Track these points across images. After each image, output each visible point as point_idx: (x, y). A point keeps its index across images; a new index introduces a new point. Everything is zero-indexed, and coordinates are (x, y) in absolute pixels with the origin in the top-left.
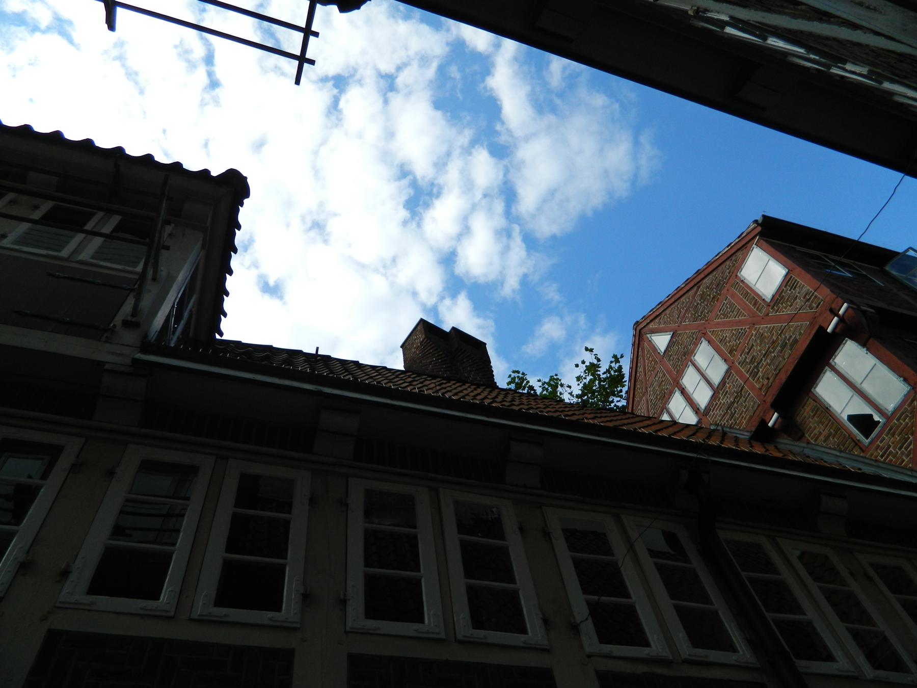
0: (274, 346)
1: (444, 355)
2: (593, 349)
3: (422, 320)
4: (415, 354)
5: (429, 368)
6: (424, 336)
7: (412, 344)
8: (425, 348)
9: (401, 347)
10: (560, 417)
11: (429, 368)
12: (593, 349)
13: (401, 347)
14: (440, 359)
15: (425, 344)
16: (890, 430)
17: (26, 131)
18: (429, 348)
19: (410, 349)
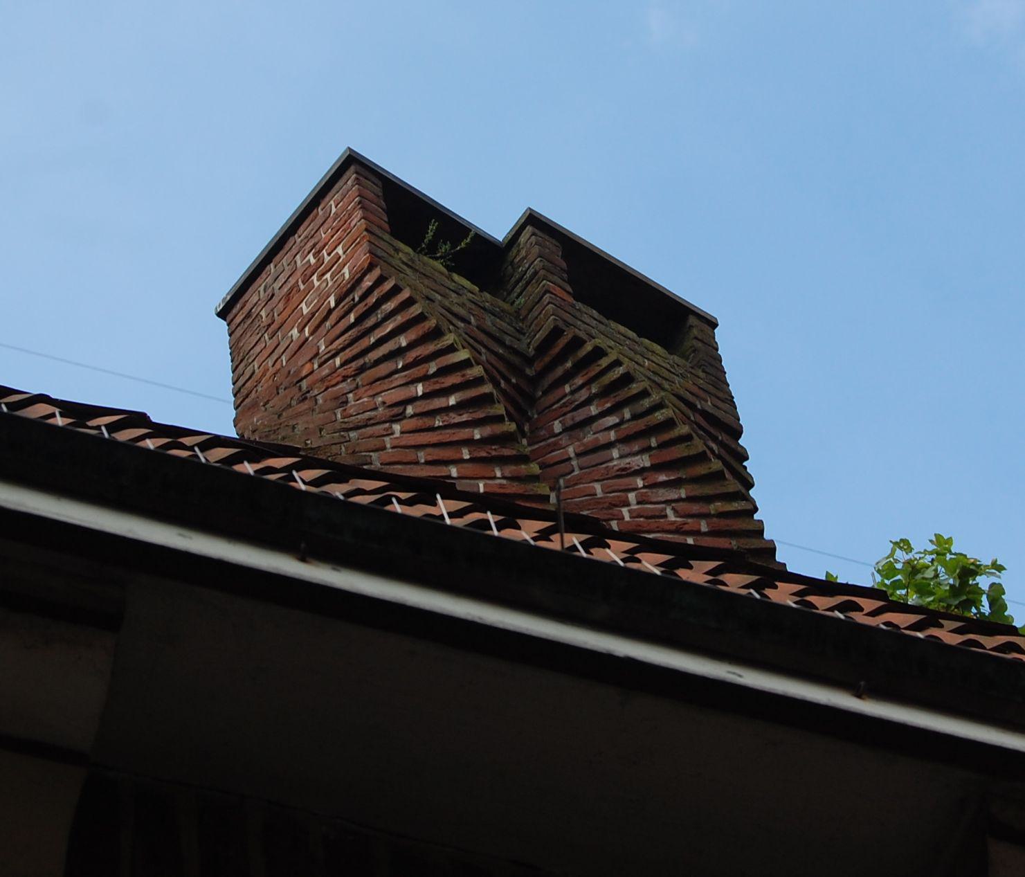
0: (849, 583)
1: (477, 371)
2: (1005, 569)
3: (352, 161)
4: (307, 353)
5: (388, 441)
6: (362, 258)
7: (288, 297)
8: (370, 322)
9: (222, 314)
10: (51, 421)
11: (388, 441)
12: (1005, 569)
13: (222, 314)
14: (424, 378)
15: (372, 299)
16: (314, 245)
17: (847, 584)
18: (389, 327)
19: (275, 328)
